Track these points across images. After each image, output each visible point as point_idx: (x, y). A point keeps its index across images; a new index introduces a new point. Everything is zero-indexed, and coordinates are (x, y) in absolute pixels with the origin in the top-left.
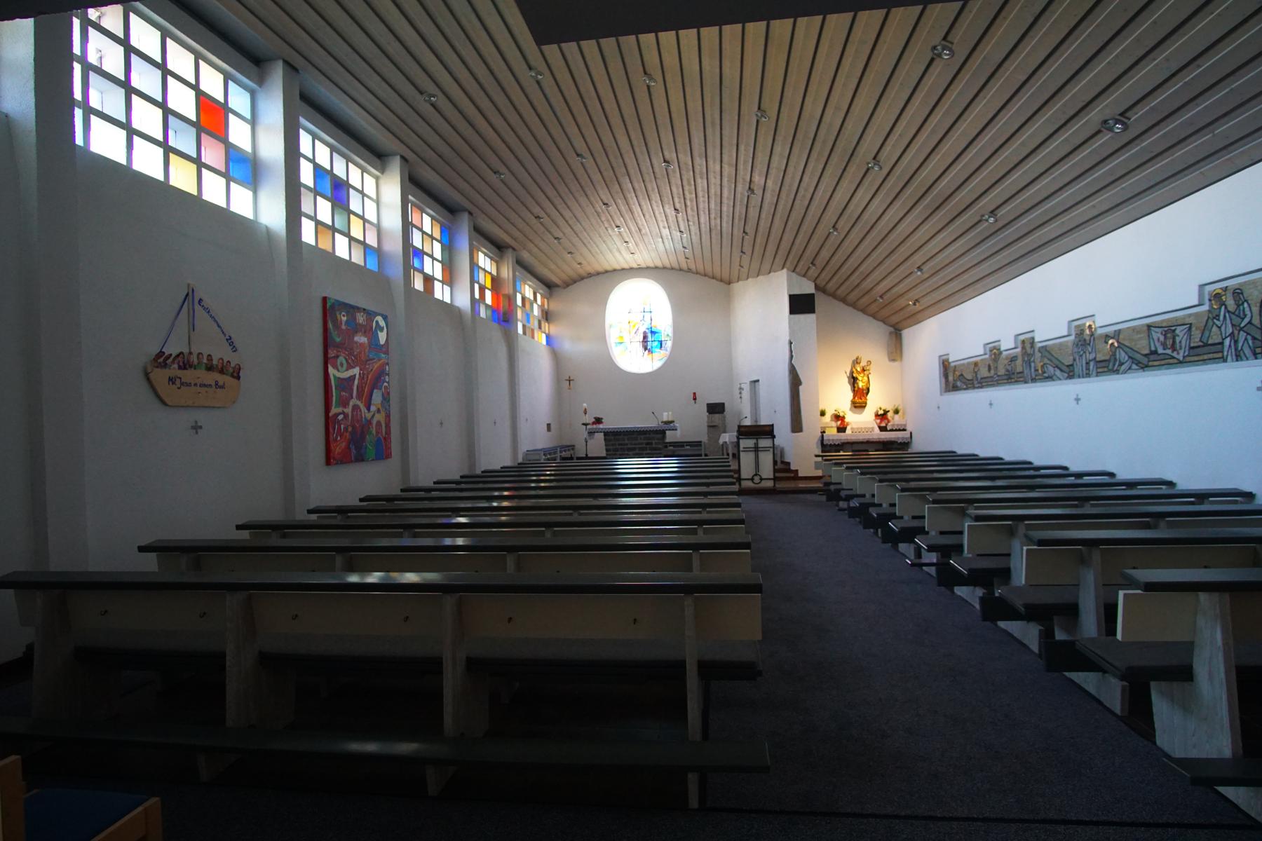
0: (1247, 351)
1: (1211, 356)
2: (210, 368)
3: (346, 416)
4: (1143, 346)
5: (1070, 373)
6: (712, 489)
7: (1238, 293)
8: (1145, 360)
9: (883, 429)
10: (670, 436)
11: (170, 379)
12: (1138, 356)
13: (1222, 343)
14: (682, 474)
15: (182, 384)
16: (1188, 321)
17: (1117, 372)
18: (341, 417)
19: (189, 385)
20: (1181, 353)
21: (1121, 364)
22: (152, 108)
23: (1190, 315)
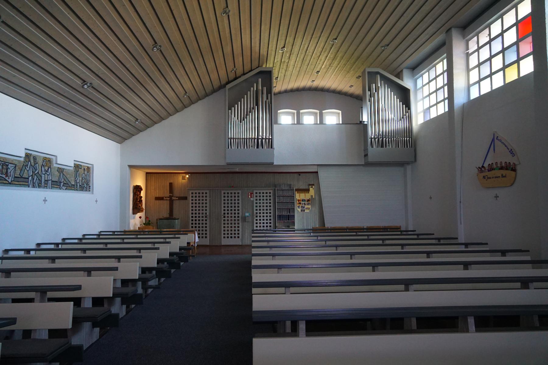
0: (37, 185)
1: (24, 183)
2: (502, 168)
6: (267, 235)
11: (484, 177)
13: (28, 179)
15: (488, 178)
16: (16, 163)
19: (490, 178)
20: (11, 178)
22: (486, 64)
23: (16, 160)
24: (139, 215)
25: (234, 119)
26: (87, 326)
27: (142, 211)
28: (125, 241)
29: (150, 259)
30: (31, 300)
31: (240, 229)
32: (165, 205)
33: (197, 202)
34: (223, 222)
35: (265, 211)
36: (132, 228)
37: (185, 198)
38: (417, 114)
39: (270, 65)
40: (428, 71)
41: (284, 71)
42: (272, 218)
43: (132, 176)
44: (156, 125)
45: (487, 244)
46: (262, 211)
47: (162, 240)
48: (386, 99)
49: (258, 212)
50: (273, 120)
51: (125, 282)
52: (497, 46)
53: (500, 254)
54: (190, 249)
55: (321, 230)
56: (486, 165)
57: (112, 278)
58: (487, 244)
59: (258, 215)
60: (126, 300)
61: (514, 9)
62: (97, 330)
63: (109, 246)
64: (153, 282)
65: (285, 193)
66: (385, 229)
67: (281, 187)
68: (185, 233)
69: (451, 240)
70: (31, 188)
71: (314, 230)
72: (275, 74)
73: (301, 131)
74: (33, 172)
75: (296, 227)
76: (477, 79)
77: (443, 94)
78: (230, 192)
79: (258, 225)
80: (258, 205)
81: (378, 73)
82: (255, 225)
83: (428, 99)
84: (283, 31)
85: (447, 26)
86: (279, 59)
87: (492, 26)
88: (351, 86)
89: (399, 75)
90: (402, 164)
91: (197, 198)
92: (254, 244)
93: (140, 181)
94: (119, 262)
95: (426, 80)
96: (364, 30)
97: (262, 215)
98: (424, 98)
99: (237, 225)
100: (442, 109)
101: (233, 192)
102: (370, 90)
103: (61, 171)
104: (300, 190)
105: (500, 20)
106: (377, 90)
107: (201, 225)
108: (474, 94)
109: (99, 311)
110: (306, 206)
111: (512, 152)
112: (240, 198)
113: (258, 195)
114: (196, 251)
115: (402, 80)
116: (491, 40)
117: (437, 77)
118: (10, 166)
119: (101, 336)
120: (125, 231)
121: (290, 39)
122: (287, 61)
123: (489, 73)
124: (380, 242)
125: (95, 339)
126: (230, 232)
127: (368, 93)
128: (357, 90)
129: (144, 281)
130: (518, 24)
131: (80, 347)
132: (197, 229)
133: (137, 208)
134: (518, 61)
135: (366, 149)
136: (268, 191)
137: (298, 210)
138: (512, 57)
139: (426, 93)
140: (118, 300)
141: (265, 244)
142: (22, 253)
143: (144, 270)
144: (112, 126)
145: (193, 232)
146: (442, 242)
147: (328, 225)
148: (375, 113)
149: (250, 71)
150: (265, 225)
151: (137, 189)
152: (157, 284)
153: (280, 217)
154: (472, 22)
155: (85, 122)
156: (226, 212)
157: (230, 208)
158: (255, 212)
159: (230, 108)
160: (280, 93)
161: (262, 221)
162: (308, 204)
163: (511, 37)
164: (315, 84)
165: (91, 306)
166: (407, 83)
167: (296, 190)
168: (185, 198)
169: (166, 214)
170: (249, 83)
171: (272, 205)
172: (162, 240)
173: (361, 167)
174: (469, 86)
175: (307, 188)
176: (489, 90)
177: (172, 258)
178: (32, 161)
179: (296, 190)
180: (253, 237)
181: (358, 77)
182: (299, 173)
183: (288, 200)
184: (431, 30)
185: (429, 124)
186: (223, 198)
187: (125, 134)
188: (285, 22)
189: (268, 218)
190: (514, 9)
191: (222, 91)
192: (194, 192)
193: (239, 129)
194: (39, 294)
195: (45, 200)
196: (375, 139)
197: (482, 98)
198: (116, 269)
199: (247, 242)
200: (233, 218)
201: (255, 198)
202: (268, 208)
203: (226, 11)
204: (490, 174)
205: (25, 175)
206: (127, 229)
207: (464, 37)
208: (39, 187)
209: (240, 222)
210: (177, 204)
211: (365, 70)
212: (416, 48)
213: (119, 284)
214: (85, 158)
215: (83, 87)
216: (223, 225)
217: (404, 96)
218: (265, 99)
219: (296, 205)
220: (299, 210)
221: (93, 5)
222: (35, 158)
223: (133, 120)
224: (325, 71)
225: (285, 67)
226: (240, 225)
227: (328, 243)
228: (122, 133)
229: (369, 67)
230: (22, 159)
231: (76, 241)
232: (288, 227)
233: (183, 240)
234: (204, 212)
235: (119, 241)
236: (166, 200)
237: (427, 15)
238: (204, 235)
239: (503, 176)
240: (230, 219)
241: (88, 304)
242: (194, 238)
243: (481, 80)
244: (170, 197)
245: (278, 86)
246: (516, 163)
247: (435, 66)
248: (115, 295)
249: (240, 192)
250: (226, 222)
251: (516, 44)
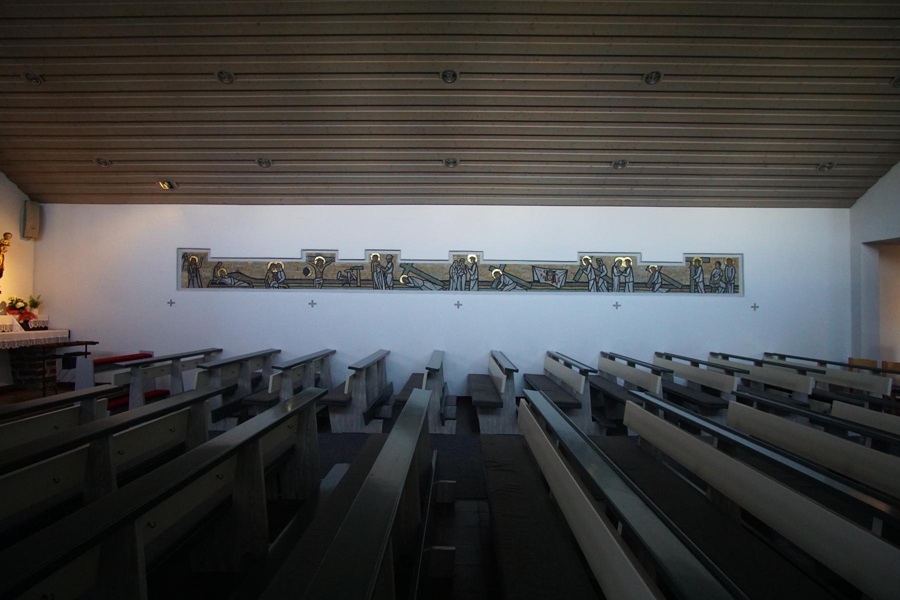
0: (604, 288)
4: (528, 276)
5: (445, 286)
7: (599, 261)
8: (529, 285)
9: (25, 326)
14: (109, 401)
16: (568, 268)
17: (502, 290)
21: (505, 285)
70: (384, 290)
118: (557, 272)
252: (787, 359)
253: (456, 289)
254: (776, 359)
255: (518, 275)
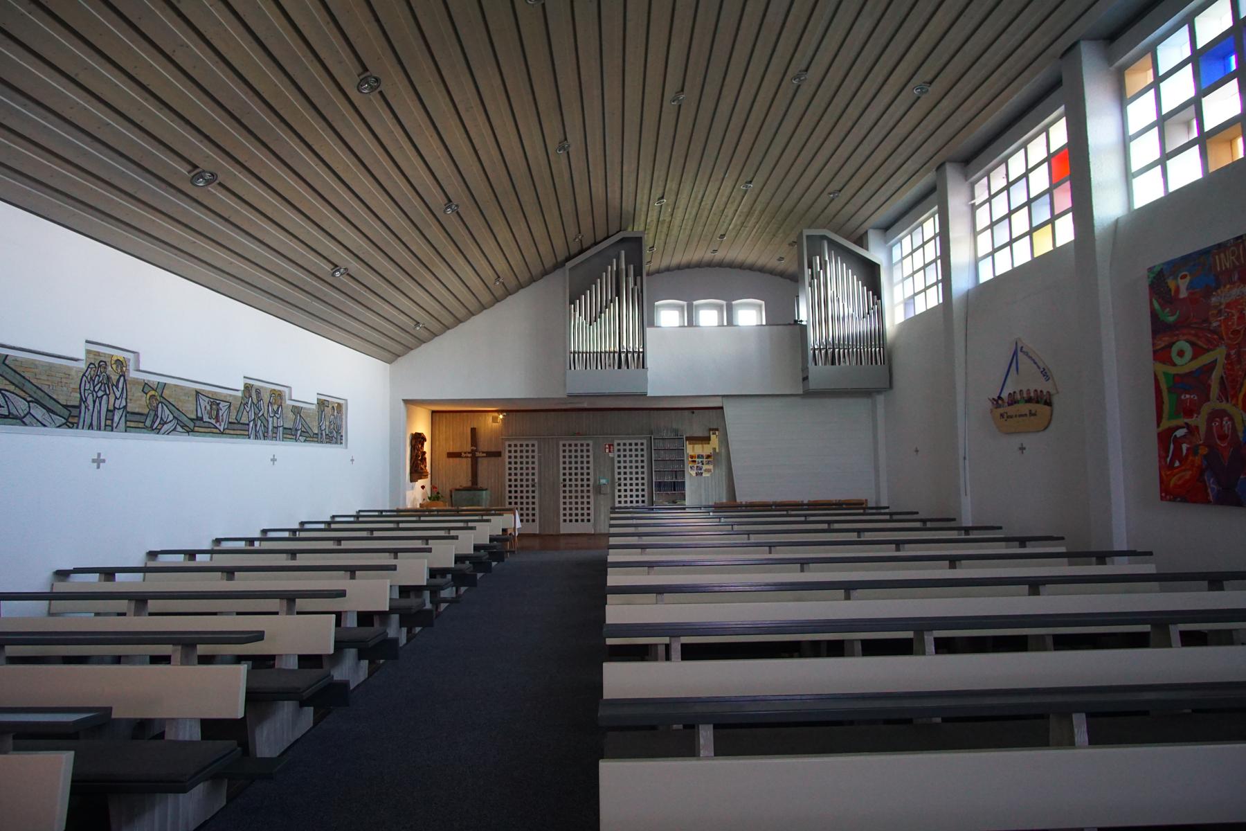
2: (1029, 400)
3: (1192, 430)
5: (70, 417)
8: (191, 425)
10: (1205, 583)
11: (1002, 415)
12: (184, 419)
17: (158, 431)
18: (1180, 433)
19: (1011, 417)
21: (163, 423)
24: (420, 482)
25: (579, 320)
26: (286, 709)
27: (426, 476)
28: (401, 525)
29: (444, 554)
30: (166, 660)
31: (592, 506)
32: (465, 464)
33: (519, 460)
34: (562, 495)
35: (634, 476)
36: (409, 506)
37: (498, 454)
38: (893, 307)
39: (639, 227)
40: (911, 233)
41: (663, 237)
42: (645, 487)
43: (409, 416)
44: (449, 332)
45: (1000, 528)
46: (628, 476)
47: (461, 525)
48: (840, 282)
49: (622, 476)
50: (646, 320)
51: (405, 591)
52: (1019, 196)
53: (1205, 583)
54: (507, 540)
55: (730, 507)
56: (1005, 395)
57: (388, 583)
58: (1000, 528)
59: (623, 482)
60: (409, 618)
61: (1186, 28)
62: (365, 663)
63: (376, 534)
64: (447, 593)
65: (668, 445)
66: (839, 505)
67: (665, 433)
68: (500, 512)
69: (946, 522)
70: (252, 441)
71: (718, 508)
72: (648, 240)
73: (694, 340)
74: (106, 395)
75: (687, 502)
76: (990, 250)
77: (933, 274)
78: (573, 443)
79: (623, 499)
80: (622, 465)
81: (824, 237)
82: (617, 499)
83: (910, 283)
84: (660, 173)
85: (937, 160)
86: (655, 219)
87: (1029, 146)
88: (781, 259)
89: (862, 241)
90: (868, 393)
91: (519, 454)
92: (613, 530)
93: (422, 426)
94: (396, 558)
95: (907, 248)
96: (806, 155)
97: (628, 482)
98: (904, 279)
99: (585, 500)
100: (933, 299)
101: (579, 443)
102: (810, 266)
103: (297, 411)
104: (693, 440)
105: (1185, 29)
106: (823, 266)
107: (525, 500)
108: (986, 275)
109: (366, 632)
110: (705, 467)
111: (1045, 374)
112: (591, 454)
113: (622, 447)
114: (517, 544)
115: (867, 249)
116: (1009, 185)
117: (924, 243)
118: (222, 404)
119: (370, 674)
120: (398, 511)
121: (672, 185)
122: (668, 220)
123: (1008, 240)
124: (825, 526)
125: (362, 679)
126: (574, 512)
127: (808, 272)
128: (788, 265)
129: (434, 590)
130: (1050, 158)
131: (345, 684)
132: (519, 506)
133: (417, 471)
134: (1051, 221)
135: (805, 369)
136: (639, 442)
137: (690, 473)
138: (1042, 214)
139: (908, 270)
140: (395, 618)
141: (631, 530)
142: (241, 545)
143: (434, 573)
144: (375, 334)
145: (512, 511)
146: (895, 517)
147: (740, 499)
148: (821, 304)
149: (605, 239)
150: (634, 499)
151: (418, 439)
152: (454, 595)
153: (660, 485)
154: (977, 155)
155: (335, 330)
156: (567, 477)
157: (573, 471)
158: (617, 477)
159: (572, 302)
160: (658, 272)
161: (628, 493)
162: (708, 463)
163: (1040, 180)
164: (719, 256)
165: (355, 625)
166: (875, 254)
167: (687, 439)
168: (498, 454)
169: (464, 480)
170: (605, 258)
171: (645, 464)
172: (461, 525)
173: (798, 399)
174: (977, 261)
175: (706, 435)
176: (991, 277)
177: (477, 554)
178: (254, 396)
179: (687, 439)
180: (612, 526)
181: (792, 244)
182: (692, 410)
183: (674, 456)
184: (910, 166)
185: (915, 324)
186: (561, 454)
187: (397, 348)
188: (662, 157)
189: (640, 487)
190: (1186, 28)
191: (558, 272)
192: (513, 443)
193: (589, 336)
194: (285, 602)
195: (274, 460)
196: (820, 350)
197: (998, 281)
198: (394, 568)
199: (603, 529)
200: (579, 488)
201: (617, 453)
202: (640, 470)
203: (563, 144)
204: (1011, 410)
205: (244, 420)
206: (401, 507)
207: (966, 177)
208: (265, 437)
209: (591, 494)
210: (484, 464)
211: (801, 233)
212: (889, 194)
213: (396, 595)
214: (334, 390)
215: (333, 275)
216: (562, 500)
217: (871, 276)
218: (631, 285)
219: (688, 465)
220: (693, 473)
221: (323, 112)
222: (258, 392)
223: (412, 324)
224: (734, 233)
225: (665, 230)
226: (592, 500)
227: (754, 539)
228: (392, 347)
229: (809, 227)
230: (240, 394)
231: (322, 526)
232: (674, 502)
233: (484, 531)
234: (530, 477)
235: (391, 525)
236: (464, 458)
237: (963, 76)
238: (531, 518)
239: (1032, 414)
240: (573, 488)
241: (351, 622)
242: (513, 522)
243: (995, 250)
244: (473, 452)
245: (653, 261)
246: (1052, 391)
247: (921, 225)
248: (393, 610)
249: (591, 443)
250: (567, 494)
251: (1049, 192)
252: (119, 577)
253: (91, 427)
254: (92, 582)
255: (179, 405)
